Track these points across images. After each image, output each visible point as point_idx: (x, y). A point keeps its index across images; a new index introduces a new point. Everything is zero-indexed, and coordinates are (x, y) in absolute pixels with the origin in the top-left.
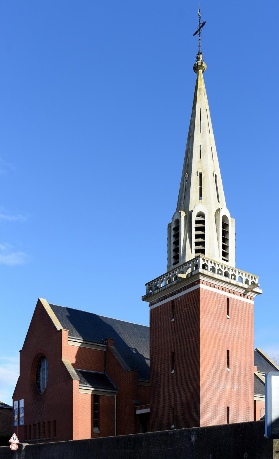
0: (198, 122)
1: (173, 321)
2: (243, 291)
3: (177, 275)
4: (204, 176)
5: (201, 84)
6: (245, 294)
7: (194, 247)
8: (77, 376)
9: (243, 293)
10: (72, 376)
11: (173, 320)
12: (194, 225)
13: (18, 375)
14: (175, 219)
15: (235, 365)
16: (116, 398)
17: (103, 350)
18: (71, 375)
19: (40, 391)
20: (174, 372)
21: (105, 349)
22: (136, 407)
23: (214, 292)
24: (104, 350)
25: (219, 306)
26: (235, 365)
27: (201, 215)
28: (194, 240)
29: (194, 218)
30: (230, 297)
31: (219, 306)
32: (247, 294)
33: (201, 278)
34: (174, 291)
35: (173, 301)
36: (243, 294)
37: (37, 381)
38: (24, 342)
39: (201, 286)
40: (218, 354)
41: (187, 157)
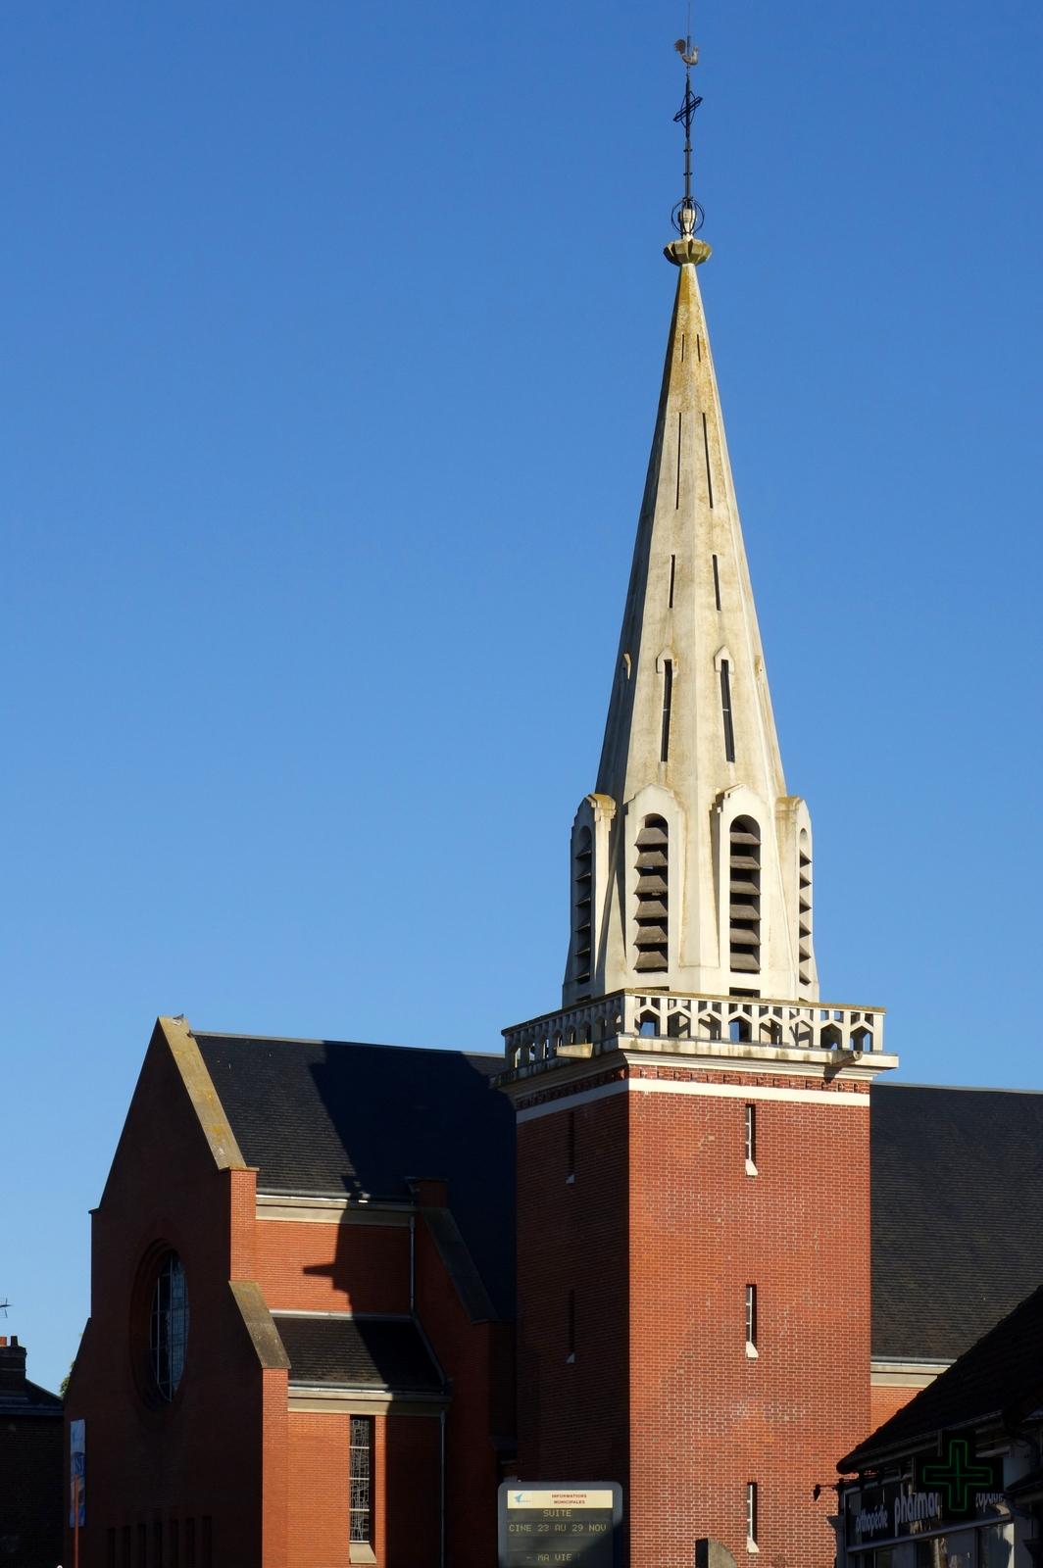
0: (669, 469)
1: (571, 1184)
2: (819, 1073)
3: (555, 1051)
4: (679, 675)
5: (695, 319)
6: (832, 1079)
7: (633, 929)
8: (280, 1353)
9: (822, 1075)
10: (259, 1353)
11: (571, 1179)
12: (632, 856)
13: (86, 1313)
14: (581, 827)
15: (782, 1333)
16: (443, 1421)
17: (404, 1225)
18: (257, 1349)
19: (166, 1388)
20: (573, 1361)
21: (412, 1219)
22: (503, 1463)
23: (687, 1095)
24: (409, 1223)
25: (711, 1138)
26: (782, 1333)
27: (656, 822)
28: (633, 904)
29: (635, 830)
30: (758, 1100)
31: (711, 1138)
32: (837, 1076)
33: (632, 1060)
34: (573, 1080)
35: (571, 1114)
36: (825, 1078)
37: (155, 1345)
38: (126, 1125)
39: (635, 1084)
40: (708, 1304)
41: (633, 593)
